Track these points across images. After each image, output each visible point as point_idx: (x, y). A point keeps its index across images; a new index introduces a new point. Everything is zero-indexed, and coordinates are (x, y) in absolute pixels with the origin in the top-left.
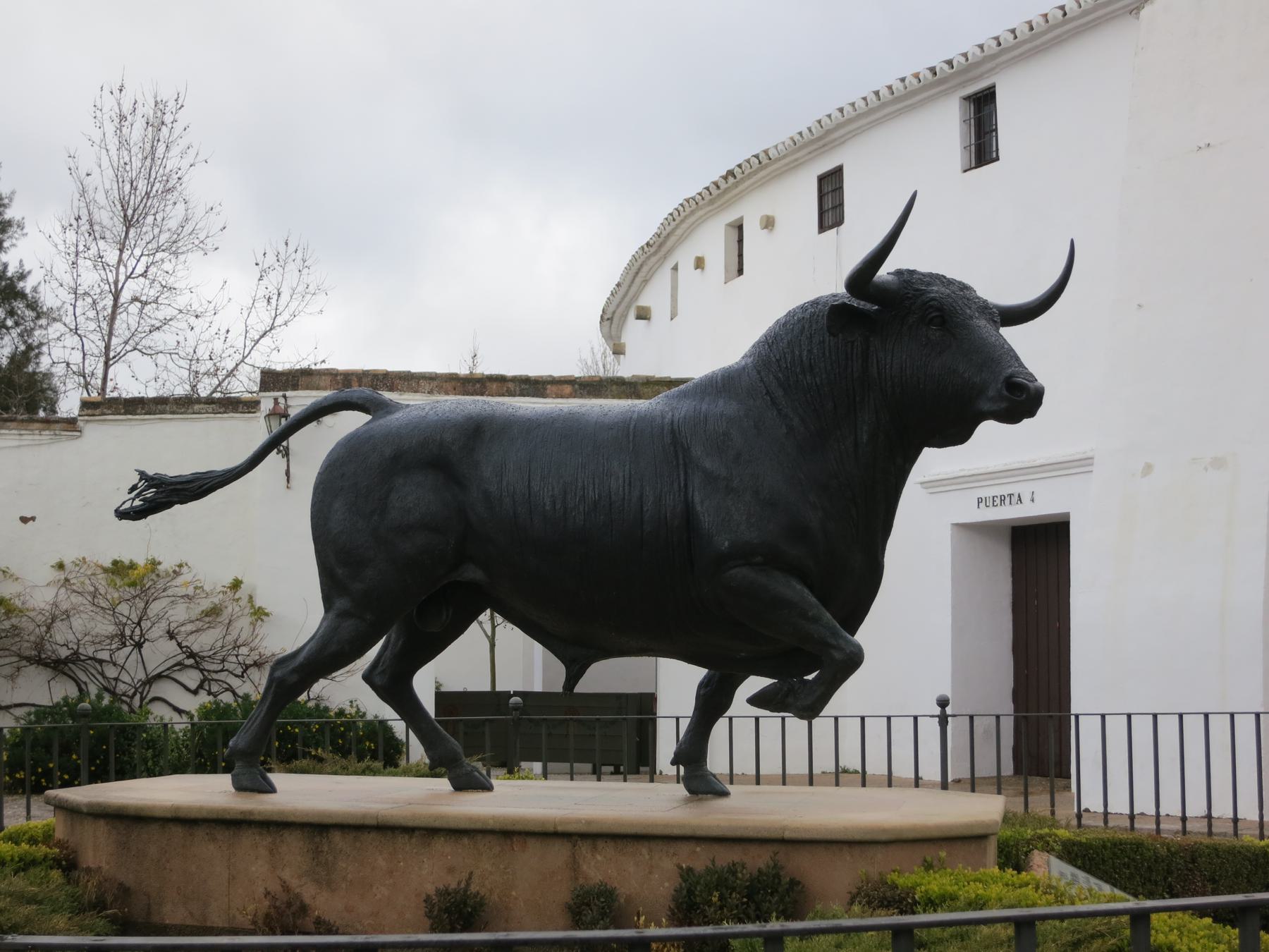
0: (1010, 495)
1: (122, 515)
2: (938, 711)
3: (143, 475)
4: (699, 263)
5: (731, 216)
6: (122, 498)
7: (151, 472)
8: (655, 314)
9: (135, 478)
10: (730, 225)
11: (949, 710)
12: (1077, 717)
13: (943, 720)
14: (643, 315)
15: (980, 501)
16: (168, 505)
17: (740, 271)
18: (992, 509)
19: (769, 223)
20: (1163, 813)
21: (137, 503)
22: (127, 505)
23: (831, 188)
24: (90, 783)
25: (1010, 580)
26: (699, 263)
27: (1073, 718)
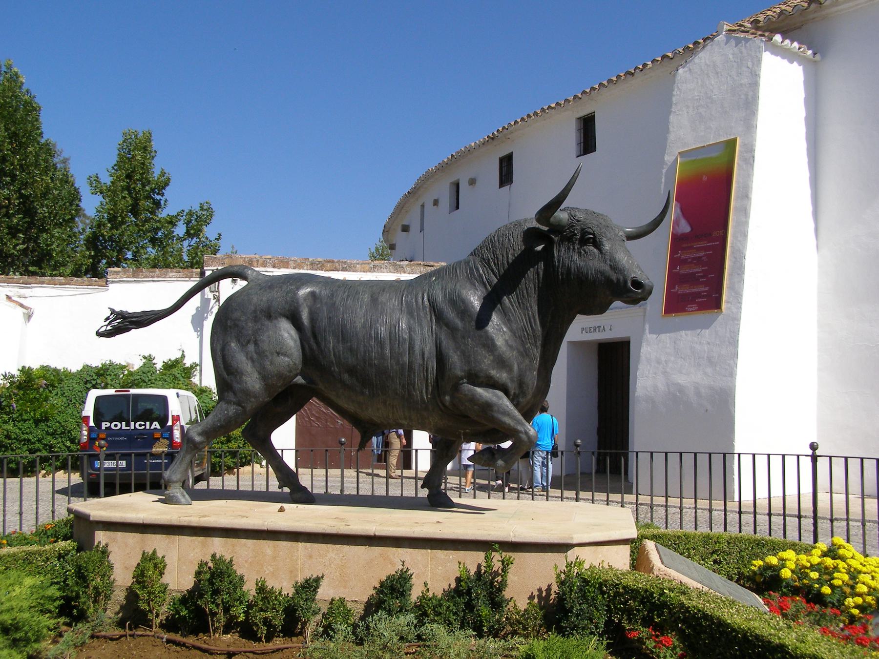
0: (599, 327)
1: (99, 334)
2: (810, 452)
3: (113, 311)
4: (436, 203)
5: (453, 179)
6: (100, 324)
7: (117, 310)
8: (412, 229)
9: (108, 313)
10: (452, 183)
11: (818, 452)
12: (416, 451)
13: (814, 459)
14: (405, 229)
15: (583, 329)
16: (128, 330)
17: (457, 208)
18: (589, 334)
19: (472, 182)
20: (867, 518)
21: (109, 328)
22: (103, 329)
23: (506, 165)
24: (120, 494)
25: (597, 372)
26: (436, 203)
27: (414, 452)
